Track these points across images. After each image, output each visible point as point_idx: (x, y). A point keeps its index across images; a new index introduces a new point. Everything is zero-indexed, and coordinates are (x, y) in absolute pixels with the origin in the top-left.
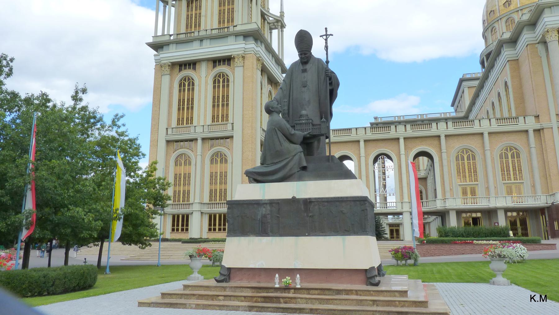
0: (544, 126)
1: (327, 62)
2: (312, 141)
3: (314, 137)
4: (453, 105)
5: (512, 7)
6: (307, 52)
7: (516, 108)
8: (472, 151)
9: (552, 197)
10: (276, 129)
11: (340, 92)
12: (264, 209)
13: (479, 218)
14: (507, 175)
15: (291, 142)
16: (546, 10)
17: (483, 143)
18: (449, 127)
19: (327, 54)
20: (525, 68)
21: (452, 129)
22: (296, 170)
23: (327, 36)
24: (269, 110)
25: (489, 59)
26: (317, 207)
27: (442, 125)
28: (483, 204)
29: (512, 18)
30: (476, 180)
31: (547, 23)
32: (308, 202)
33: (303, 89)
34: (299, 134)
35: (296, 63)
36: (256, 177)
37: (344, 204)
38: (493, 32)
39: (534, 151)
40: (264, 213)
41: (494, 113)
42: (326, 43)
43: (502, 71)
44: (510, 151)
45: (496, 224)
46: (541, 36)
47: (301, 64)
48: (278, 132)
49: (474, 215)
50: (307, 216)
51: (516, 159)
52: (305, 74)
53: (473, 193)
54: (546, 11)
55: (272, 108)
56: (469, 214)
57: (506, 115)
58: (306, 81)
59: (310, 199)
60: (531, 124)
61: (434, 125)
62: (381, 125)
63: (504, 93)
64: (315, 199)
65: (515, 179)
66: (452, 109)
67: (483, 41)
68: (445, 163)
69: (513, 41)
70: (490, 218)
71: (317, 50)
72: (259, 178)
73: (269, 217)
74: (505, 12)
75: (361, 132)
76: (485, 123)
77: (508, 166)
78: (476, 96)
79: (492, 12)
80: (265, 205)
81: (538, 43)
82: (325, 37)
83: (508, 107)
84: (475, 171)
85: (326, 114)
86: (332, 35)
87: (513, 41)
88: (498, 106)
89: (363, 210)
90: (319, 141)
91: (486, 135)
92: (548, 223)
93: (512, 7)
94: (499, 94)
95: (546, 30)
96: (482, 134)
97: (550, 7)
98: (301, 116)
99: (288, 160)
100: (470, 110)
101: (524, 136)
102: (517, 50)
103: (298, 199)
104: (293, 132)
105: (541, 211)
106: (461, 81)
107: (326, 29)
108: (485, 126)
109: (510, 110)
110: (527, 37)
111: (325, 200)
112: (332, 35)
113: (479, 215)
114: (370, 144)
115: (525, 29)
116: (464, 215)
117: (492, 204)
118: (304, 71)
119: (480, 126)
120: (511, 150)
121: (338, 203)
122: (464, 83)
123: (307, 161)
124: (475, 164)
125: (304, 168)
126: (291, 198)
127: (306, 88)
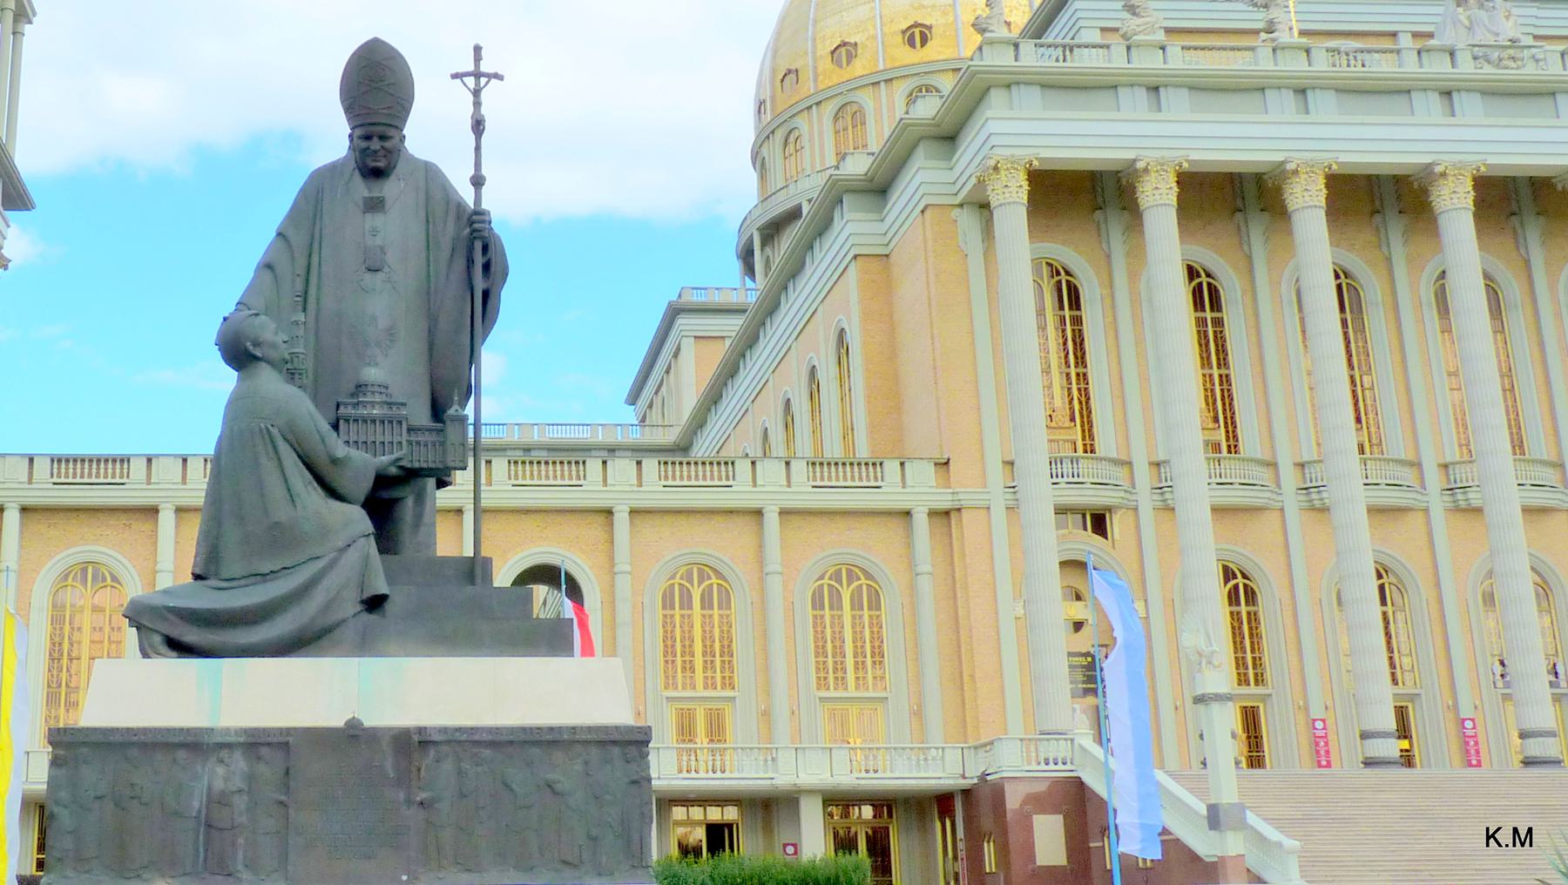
0: (966, 499)
1: (478, 182)
2: (396, 493)
3: (410, 475)
4: (633, 399)
5: (859, 67)
6: (392, 132)
7: (872, 428)
8: (868, 576)
9: (981, 752)
10: (275, 431)
11: (510, 297)
12: (220, 770)
13: (730, 826)
14: (723, 670)
15: (333, 493)
16: (993, 92)
17: (761, 547)
18: (794, 479)
19: (478, 149)
20: (911, 287)
21: (655, 485)
22: (351, 606)
23: (478, 77)
24: (239, 352)
25: (779, 238)
26: (448, 766)
27: (622, 468)
28: (748, 773)
29: (855, 108)
30: (729, 683)
31: (994, 141)
32: (413, 745)
33: (368, 276)
34: (361, 464)
35: (331, 171)
36: (178, 633)
37: (558, 756)
38: (791, 147)
39: (925, 585)
40: (219, 785)
41: (790, 440)
42: (477, 104)
43: (829, 292)
44: (700, 583)
45: (790, 850)
46: (973, 181)
47: (357, 177)
48: (284, 448)
49: (715, 815)
50: (409, 802)
51: (866, 613)
52: (376, 220)
53: (716, 730)
54: (996, 97)
55: (256, 344)
56: (697, 813)
57: (834, 450)
58: (382, 248)
59: (421, 730)
60: (919, 489)
61: (594, 466)
62: (543, 456)
63: (833, 369)
64: (444, 730)
65: (710, 684)
66: (630, 415)
67: (753, 176)
68: (624, 612)
69: (878, 189)
70: (768, 828)
71: (431, 132)
72: (191, 636)
73: (240, 802)
74: (835, 80)
75: (167, 472)
76: (771, 472)
77: (839, 638)
78: (730, 371)
79: (793, 76)
80: (224, 754)
81: (961, 205)
82: (470, 81)
83: (850, 420)
84: (727, 650)
85: (447, 391)
86: (498, 76)
87: (878, 189)
88: (807, 417)
89: (634, 782)
90: (420, 498)
91: (772, 518)
92: (961, 845)
93: (859, 67)
94: (813, 371)
95: (992, 163)
96: (758, 513)
97: (1009, 86)
98: (360, 388)
99: (320, 564)
100: (699, 422)
101: (895, 527)
102: (889, 220)
103: (374, 729)
104: (341, 451)
105: (943, 802)
106: (674, 312)
107: (477, 50)
108: (769, 486)
109: (848, 431)
110: (925, 177)
111: (485, 737)
112: (498, 76)
113: (731, 814)
114: (796, 521)
115: (920, 153)
116: (679, 813)
117: (783, 775)
118: (375, 205)
119: (755, 485)
120: (851, 577)
121: (536, 751)
122: (683, 322)
123: (391, 580)
124: (876, 624)
125: (375, 603)
126: (338, 721)
127: (380, 275)
